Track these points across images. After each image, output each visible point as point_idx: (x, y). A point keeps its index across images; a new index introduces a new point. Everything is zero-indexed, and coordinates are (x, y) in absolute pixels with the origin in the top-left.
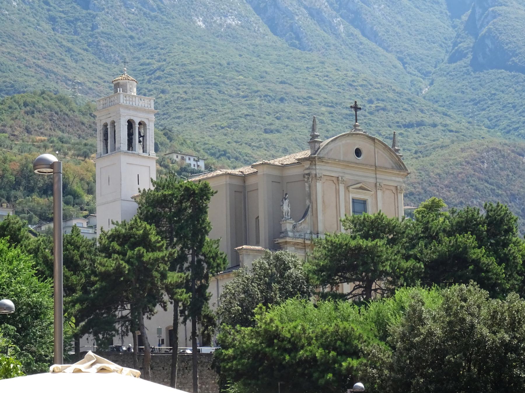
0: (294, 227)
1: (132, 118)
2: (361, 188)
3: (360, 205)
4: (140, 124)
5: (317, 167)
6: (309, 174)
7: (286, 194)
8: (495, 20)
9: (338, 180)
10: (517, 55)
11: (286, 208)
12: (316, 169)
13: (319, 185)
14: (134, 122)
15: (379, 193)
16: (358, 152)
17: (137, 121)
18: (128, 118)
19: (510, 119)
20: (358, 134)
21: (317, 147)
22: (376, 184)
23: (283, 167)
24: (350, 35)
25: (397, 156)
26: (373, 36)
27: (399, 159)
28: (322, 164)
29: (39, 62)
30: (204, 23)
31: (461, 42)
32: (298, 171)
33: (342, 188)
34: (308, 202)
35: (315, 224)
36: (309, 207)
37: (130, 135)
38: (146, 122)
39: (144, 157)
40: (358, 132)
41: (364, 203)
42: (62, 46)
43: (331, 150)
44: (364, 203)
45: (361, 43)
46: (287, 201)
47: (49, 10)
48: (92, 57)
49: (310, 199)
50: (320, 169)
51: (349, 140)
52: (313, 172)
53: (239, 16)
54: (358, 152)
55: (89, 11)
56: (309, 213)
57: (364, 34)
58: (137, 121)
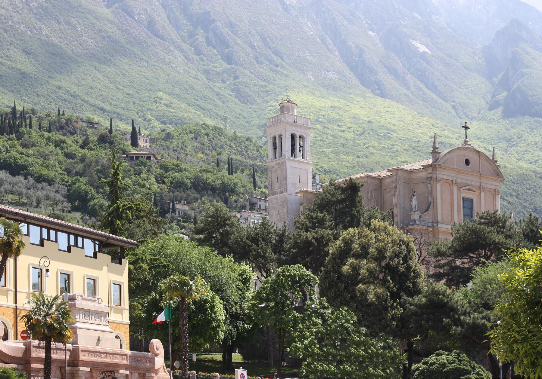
0: (420, 217)
1: (294, 132)
2: (469, 190)
3: (468, 204)
4: (300, 137)
5: (438, 172)
6: (431, 178)
7: (415, 192)
8: (523, 79)
9: (452, 183)
10: (539, 105)
11: (414, 203)
12: (436, 174)
13: (439, 186)
14: (295, 135)
15: (483, 194)
16: (467, 162)
17: (298, 135)
18: (291, 132)
19: (532, 154)
20: (467, 148)
21: (437, 157)
22: (480, 187)
23: (411, 172)
24: (419, 89)
25: (496, 166)
26: (434, 89)
27: (498, 168)
28: (441, 170)
29: (198, 103)
30: (313, 76)
31: (498, 94)
32: (423, 174)
33: (455, 189)
34: (430, 198)
35: (435, 215)
36: (431, 202)
37: (293, 145)
38: (305, 135)
39: (303, 162)
40: (467, 146)
41: (471, 201)
42: (213, 91)
43: (448, 159)
44: (471, 201)
45: (425, 94)
46: (415, 197)
47: (204, 65)
48: (234, 99)
49: (432, 196)
50: (441, 174)
51: (461, 152)
52: (434, 176)
53: (337, 72)
54: (467, 162)
55: (232, 66)
56: (431, 207)
57: (427, 87)
58: (298, 135)
